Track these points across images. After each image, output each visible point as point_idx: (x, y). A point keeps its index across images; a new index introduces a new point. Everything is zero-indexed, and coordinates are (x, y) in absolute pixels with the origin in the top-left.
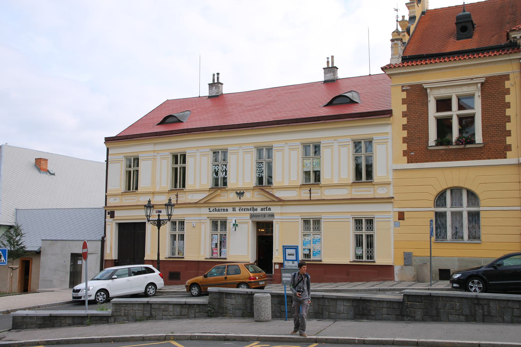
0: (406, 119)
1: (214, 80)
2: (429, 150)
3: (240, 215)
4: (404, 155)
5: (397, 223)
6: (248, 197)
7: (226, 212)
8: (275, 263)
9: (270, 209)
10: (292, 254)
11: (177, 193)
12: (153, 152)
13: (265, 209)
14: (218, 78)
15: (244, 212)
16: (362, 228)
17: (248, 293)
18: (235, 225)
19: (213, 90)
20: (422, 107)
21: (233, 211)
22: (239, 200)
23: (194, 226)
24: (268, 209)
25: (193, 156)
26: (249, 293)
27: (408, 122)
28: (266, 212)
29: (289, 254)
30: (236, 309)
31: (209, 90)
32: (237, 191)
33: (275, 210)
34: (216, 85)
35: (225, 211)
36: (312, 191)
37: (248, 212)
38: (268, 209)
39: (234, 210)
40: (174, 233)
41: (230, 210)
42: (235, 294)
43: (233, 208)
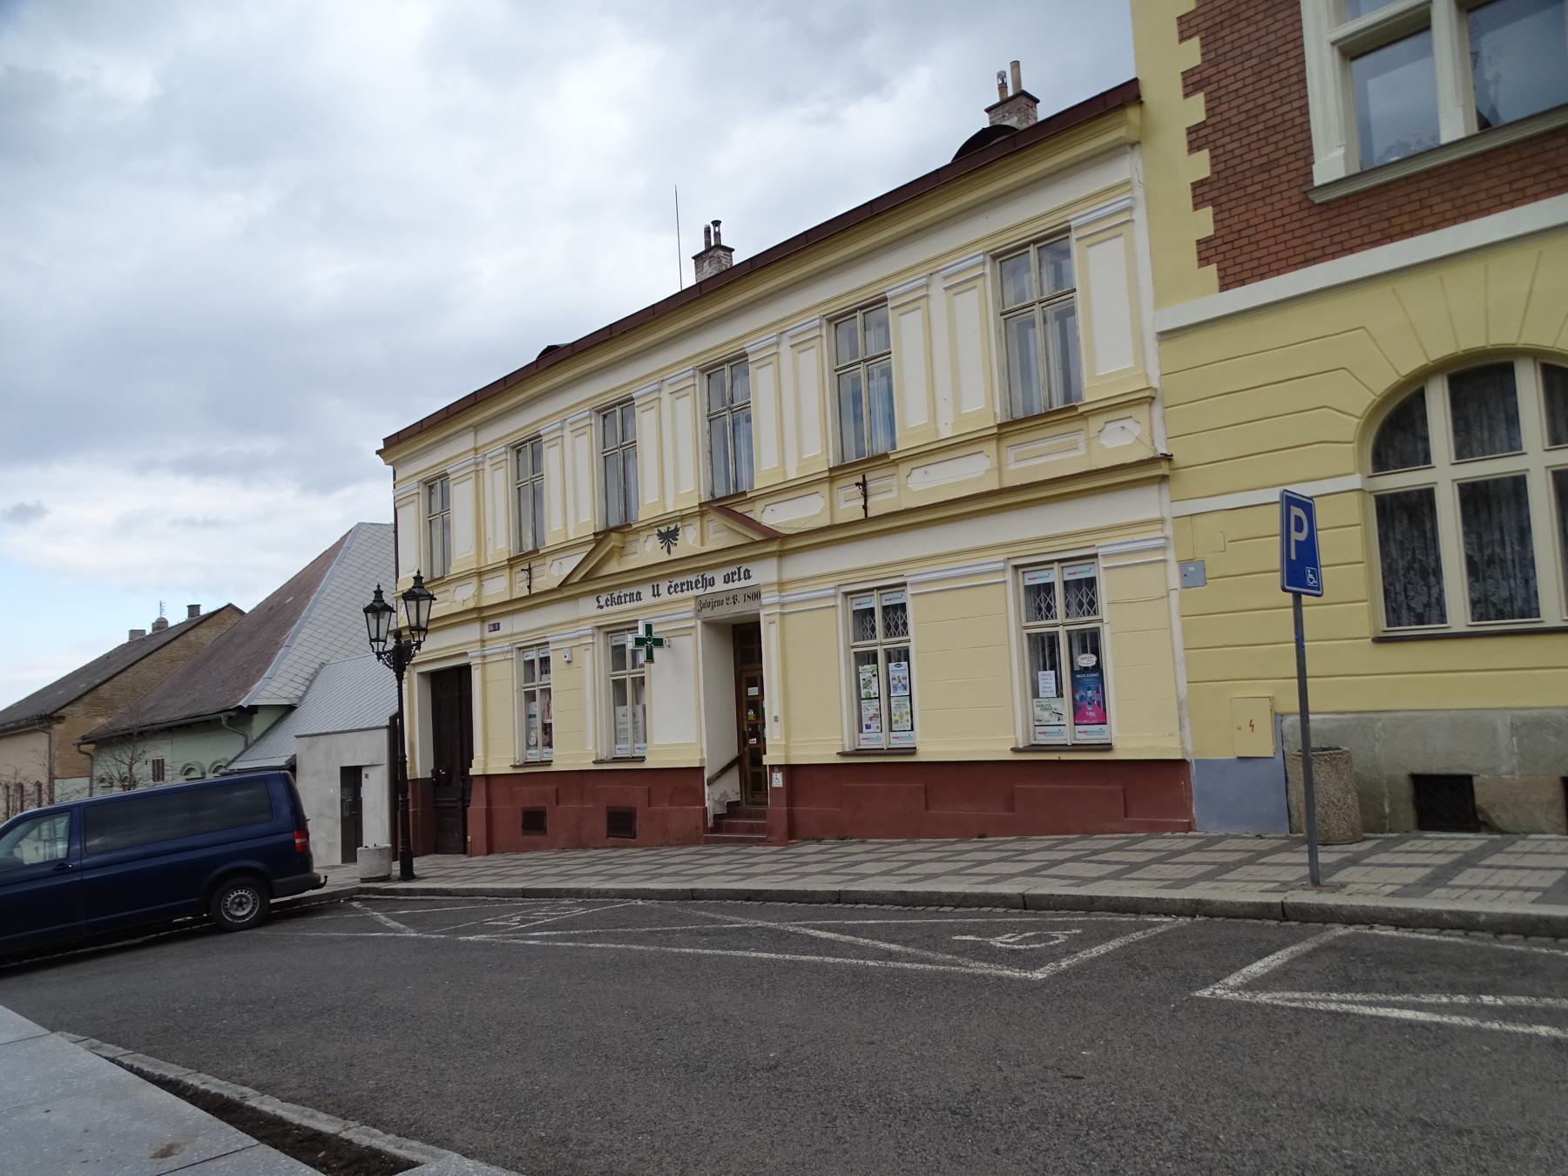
0: (1199, 99)
2: (1319, 204)
3: (962, 557)
4: (1203, 260)
5: (1192, 569)
7: (636, 604)
8: (772, 767)
9: (748, 576)
11: (864, 477)
13: (736, 577)
15: (680, 595)
16: (873, 629)
20: (1270, 21)
21: (654, 595)
22: (666, 558)
23: (567, 659)
24: (742, 576)
25: (769, 360)
27: (1212, 109)
28: (737, 585)
33: (764, 573)
36: (870, 486)
38: (742, 576)
40: (1042, 627)
43: (653, 586)
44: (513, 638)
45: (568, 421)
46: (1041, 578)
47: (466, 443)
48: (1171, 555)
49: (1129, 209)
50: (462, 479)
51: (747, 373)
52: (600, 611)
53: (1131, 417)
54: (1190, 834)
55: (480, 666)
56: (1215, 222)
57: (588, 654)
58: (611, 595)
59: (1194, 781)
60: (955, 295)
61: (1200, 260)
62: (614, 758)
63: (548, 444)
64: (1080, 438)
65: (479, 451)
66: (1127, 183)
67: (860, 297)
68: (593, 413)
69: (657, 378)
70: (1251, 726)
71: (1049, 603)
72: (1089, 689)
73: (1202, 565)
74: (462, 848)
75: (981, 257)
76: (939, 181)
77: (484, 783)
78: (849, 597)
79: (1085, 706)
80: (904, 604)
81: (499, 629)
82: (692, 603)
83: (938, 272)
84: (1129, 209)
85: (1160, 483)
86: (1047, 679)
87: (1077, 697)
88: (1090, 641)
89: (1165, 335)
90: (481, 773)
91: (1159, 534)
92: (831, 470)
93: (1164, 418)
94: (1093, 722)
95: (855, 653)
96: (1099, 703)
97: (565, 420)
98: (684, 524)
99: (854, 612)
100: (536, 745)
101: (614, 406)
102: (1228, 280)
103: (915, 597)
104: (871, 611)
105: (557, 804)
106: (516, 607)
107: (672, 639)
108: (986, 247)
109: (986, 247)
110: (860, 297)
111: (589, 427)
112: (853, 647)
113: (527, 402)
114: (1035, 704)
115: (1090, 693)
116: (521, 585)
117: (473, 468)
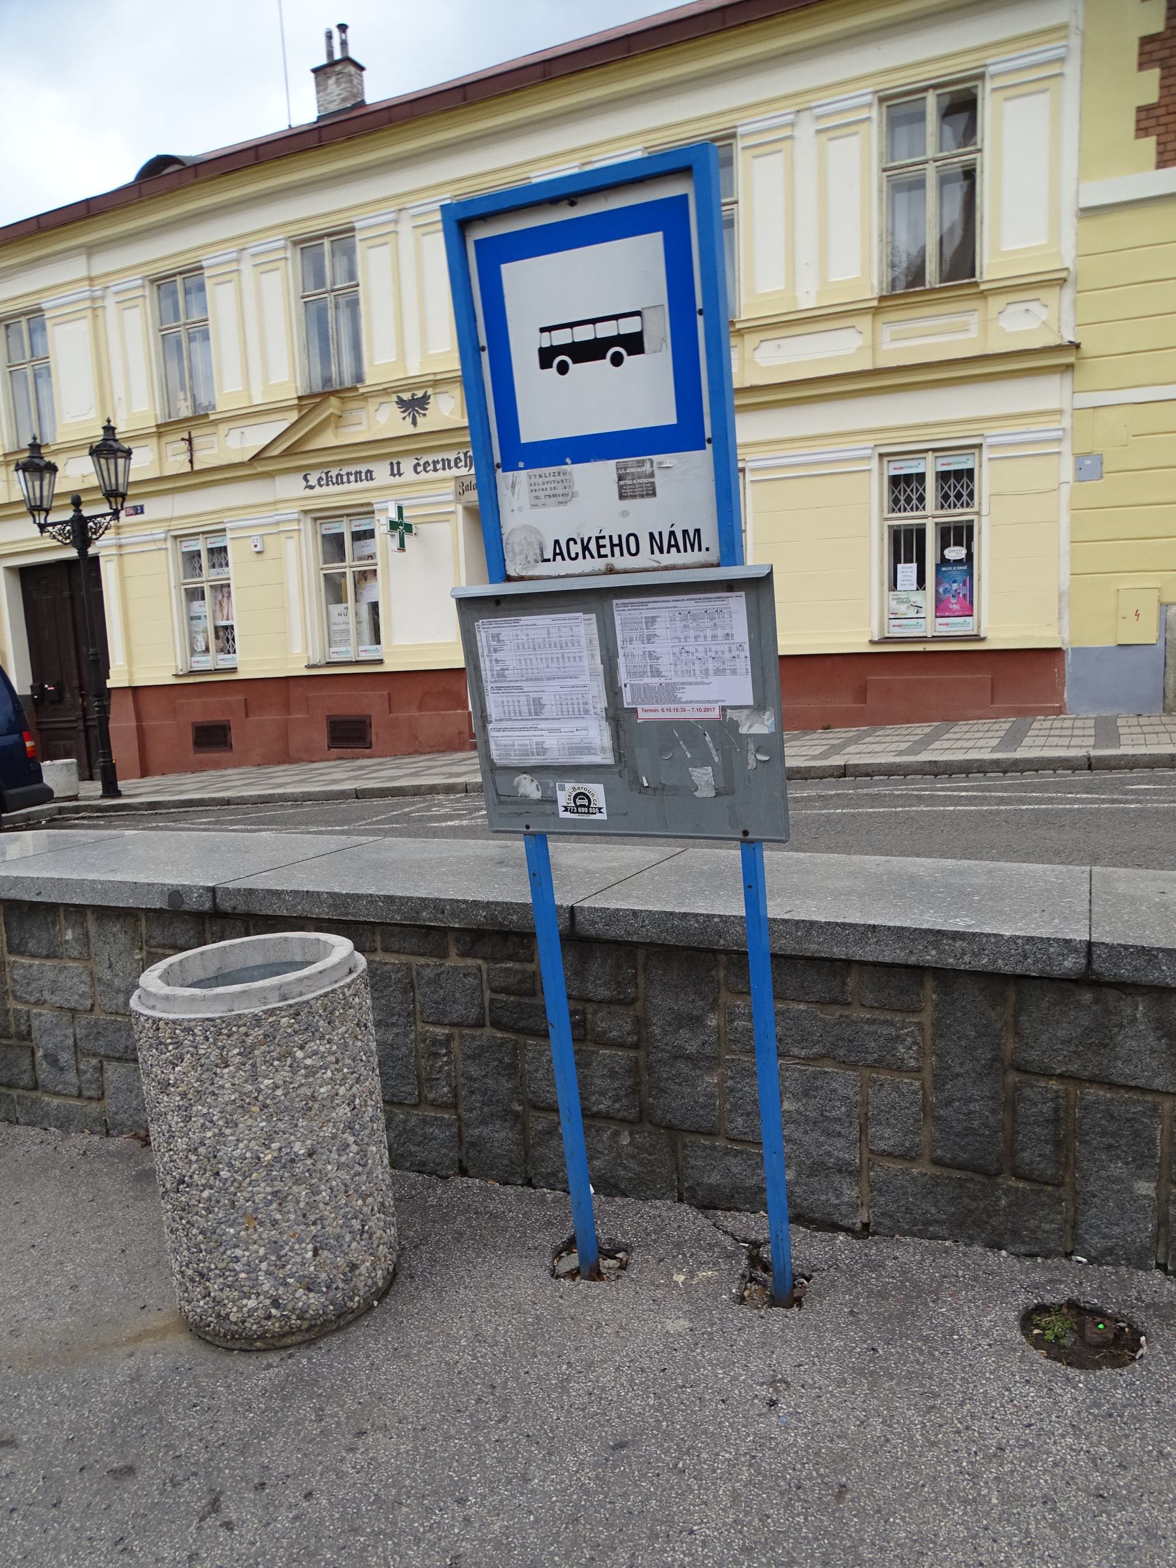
1: (330, 53)
4: (1142, 131)
5: (1088, 462)
6: (447, 414)
7: (365, 484)
10: (606, 330)
11: (190, 433)
12: (87, 283)
14: (344, 44)
15: (432, 475)
17: (185, 907)
18: (401, 527)
19: (329, 91)
21: (393, 474)
22: (411, 430)
23: (258, 549)
25: (227, 277)
26: (192, 903)
29: (562, 338)
30: (108, 1057)
31: (318, 92)
32: (399, 394)
34: (338, 68)
35: (363, 477)
36: (195, 442)
37: (449, 473)
39: (396, 472)
40: (907, 519)
41: (381, 472)
42: (81, 909)
43: (392, 464)
44: (172, 523)
45: (251, 251)
46: (334, 528)
47: (75, 268)
48: (1066, 448)
49: (1061, 60)
50: (66, 319)
51: (44, 328)
52: (309, 492)
53: (1038, 299)
54: (1061, 716)
55: (115, 558)
56: (1162, 87)
57: (291, 545)
58: (327, 473)
59: (1068, 669)
60: (755, 157)
61: (1138, 129)
62: (328, 663)
63: (999, 82)
64: (974, 320)
65: (96, 282)
66: (1063, 27)
67: (700, 128)
68: (289, 244)
69: (393, 206)
70: (1137, 615)
71: (896, 496)
72: (955, 582)
73: (1100, 459)
74: (87, 773)
75: (283, 242)
76: (629, 51)
77: (130, 698)
78: (179, 540)
79: (948, 599)
80: (373, 530)
81: (142, 512)
82: (451, 487)
83: (810, 108)
84: (1061, 60)
85: (1062, 372)
86: (908, 571)
87: (941, 590)
88: (961, 534)
89: (1088, 212)
90: (127, 685)
91: (1057, 426)
92: (158, 426)
93: (1074, 303)
94: (956, 614)
95: (325, 575)
96: (964, 596)
97: (243, 250)
98: (437, 391)
99: (183, 553)
100: (207, 649)
101: (321, 237)
102: (1167, 156)
103: (756, 485)
104: (198, 553)
105: (247, 716)
106: (178, 484)
107: (419, 526)
108: (877, 84)
109: (877, 84)
110: (700, 128)
111: (283, 261)
112: (322, 569)
113: (786, 54)
114: (891, 597)
115: (955, 586)
116: (179, 458)
117: (88, 304)
